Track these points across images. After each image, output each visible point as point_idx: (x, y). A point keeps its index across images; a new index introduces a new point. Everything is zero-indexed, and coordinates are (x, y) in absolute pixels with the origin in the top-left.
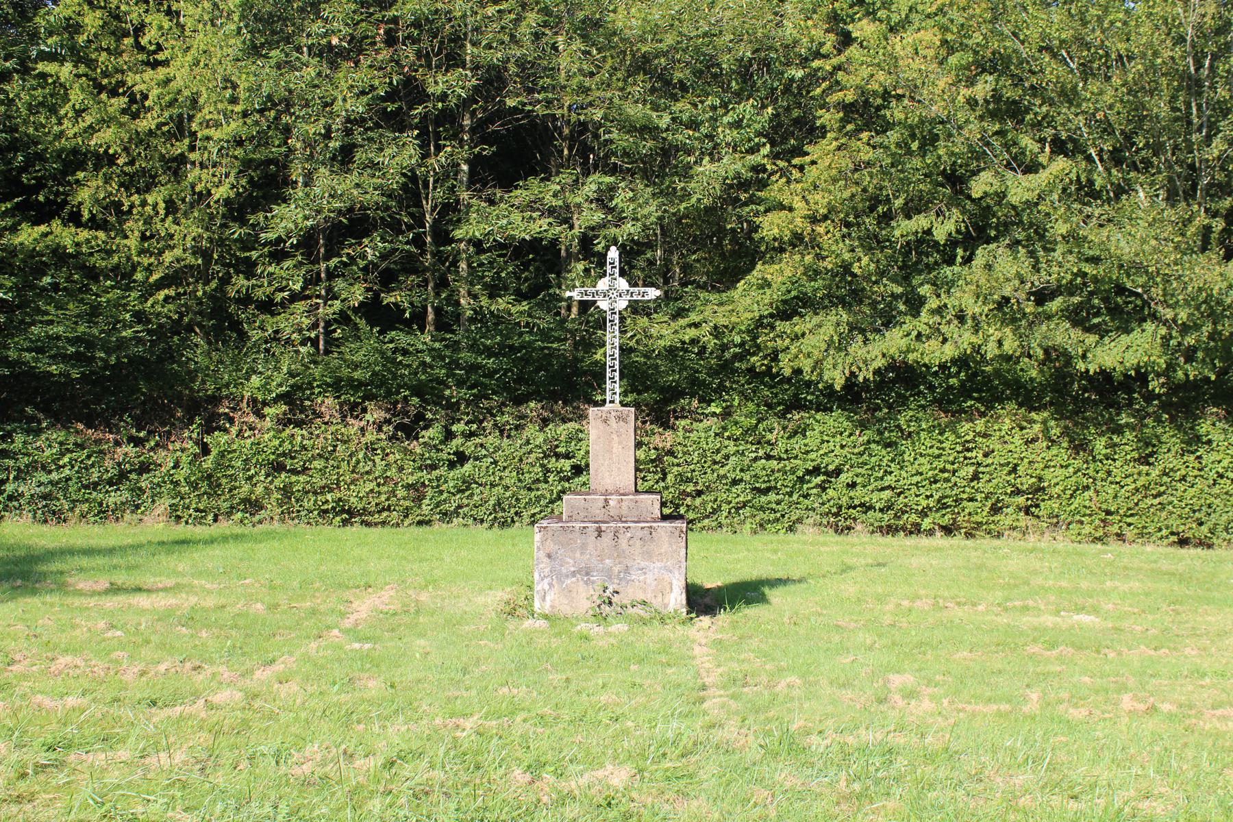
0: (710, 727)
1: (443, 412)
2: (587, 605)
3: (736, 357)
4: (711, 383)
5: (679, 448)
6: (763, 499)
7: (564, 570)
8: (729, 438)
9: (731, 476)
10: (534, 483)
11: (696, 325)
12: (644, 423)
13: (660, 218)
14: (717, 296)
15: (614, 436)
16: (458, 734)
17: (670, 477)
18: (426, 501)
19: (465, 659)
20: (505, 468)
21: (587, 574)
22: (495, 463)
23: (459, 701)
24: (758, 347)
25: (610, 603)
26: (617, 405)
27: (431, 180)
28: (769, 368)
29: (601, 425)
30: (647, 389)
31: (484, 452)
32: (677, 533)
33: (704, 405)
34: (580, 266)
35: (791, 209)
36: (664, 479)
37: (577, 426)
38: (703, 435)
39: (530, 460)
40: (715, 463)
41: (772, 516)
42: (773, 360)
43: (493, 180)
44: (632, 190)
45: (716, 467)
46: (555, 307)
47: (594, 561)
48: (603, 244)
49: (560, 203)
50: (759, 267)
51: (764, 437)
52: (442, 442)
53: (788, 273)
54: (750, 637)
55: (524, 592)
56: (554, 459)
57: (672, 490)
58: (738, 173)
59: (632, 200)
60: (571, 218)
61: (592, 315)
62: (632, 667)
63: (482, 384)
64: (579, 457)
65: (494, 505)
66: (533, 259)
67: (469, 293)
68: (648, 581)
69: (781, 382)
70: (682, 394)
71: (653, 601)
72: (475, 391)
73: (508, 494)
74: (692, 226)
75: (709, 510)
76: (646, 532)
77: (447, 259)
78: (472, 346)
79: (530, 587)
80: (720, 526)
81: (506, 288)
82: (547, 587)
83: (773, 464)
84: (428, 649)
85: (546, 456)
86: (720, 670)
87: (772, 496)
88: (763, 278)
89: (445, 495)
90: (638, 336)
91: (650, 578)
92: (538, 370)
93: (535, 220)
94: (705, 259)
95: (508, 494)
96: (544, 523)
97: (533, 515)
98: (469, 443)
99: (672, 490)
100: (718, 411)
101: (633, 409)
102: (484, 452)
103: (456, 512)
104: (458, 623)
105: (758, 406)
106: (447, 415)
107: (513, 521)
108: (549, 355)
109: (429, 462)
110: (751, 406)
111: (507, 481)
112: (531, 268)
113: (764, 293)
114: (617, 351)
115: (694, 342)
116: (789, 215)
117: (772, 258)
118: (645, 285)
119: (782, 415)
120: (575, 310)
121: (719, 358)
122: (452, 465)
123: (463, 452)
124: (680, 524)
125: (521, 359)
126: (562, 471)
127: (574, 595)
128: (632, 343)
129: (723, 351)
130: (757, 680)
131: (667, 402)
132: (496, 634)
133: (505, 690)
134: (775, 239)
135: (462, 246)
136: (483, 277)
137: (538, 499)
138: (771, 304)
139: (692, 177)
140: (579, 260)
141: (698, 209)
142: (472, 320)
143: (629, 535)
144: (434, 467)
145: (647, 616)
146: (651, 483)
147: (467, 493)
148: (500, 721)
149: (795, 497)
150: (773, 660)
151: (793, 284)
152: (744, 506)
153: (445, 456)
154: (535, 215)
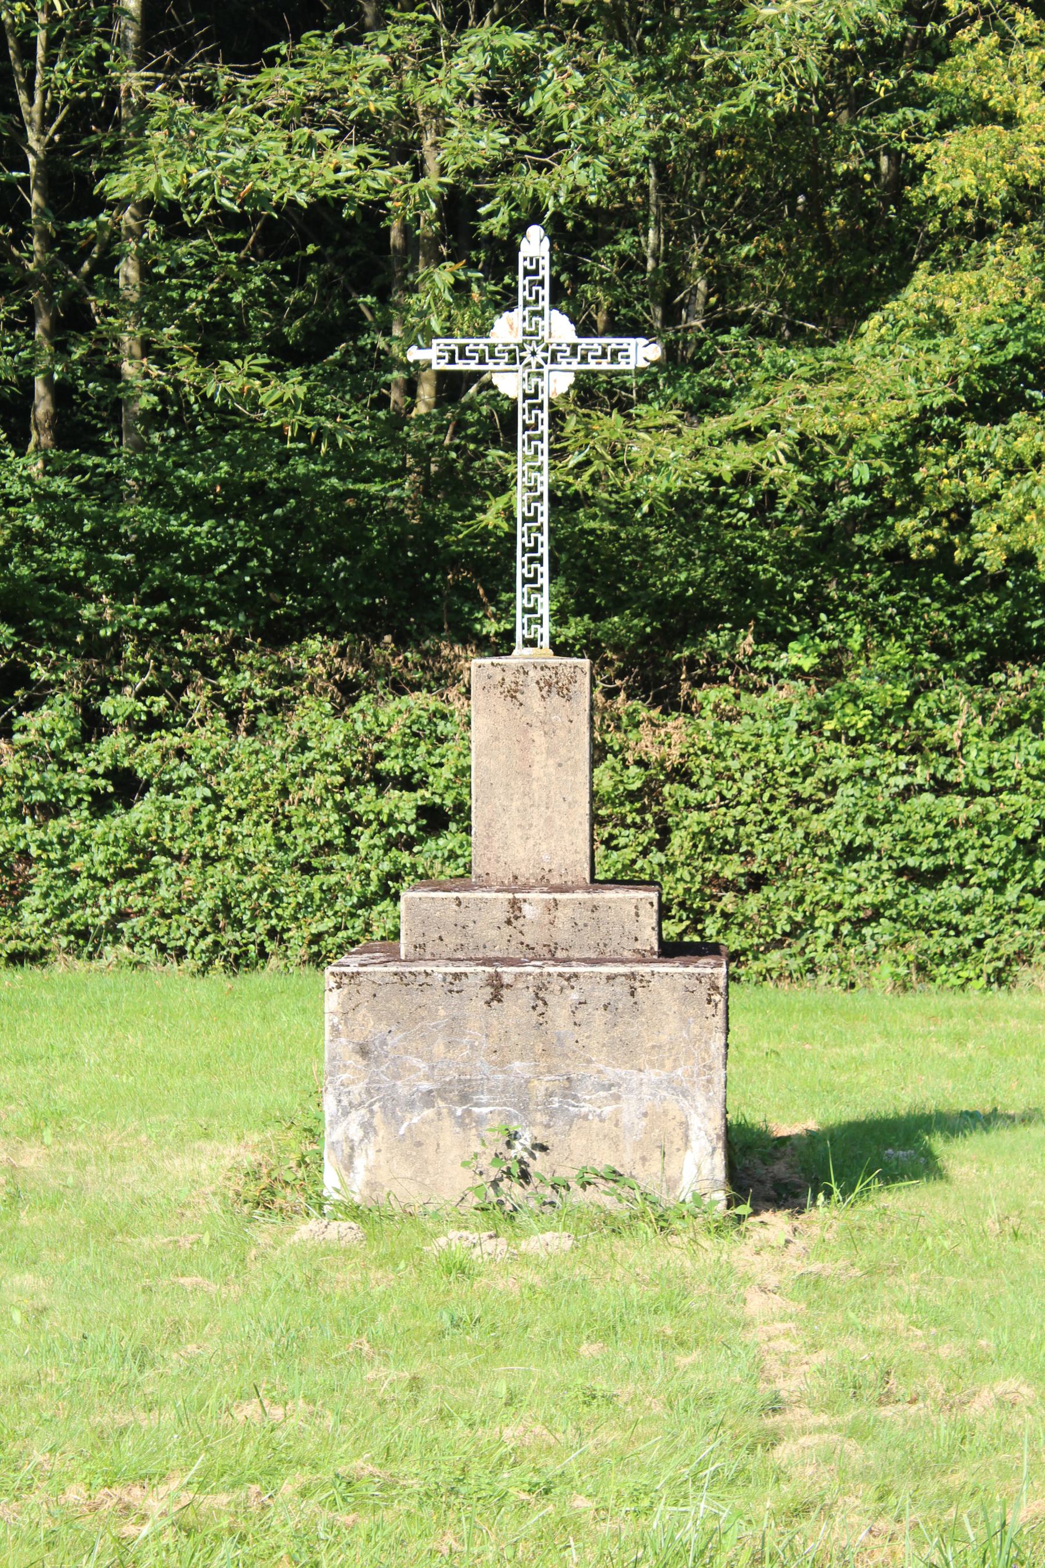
0: (796, 1513)
1: (78, 665)
2: (462, 1179)
3: (858, 520)
4: (788, 589)
5: (704, 761)
6: (927, 898)
7: (402, 1089)
8: (836, 736)
9: (842, 836)
10: (317, 852)
11: (751, 435)
12: (611, 694)
13: (657, 145)
14: (806, 356)
15: (537, 735)
16: (129, 1530)
17: (679, 840)
18: (32, 901)
19: (142, 1326)
20: (241, 813)
21: (464, 1098)
22: (216, 798)
23: (128, 1442)
24: (917, 494)
25: (525, 1176)
26: (544, 652)
27: (41, 36)
28: (946, 549)
29: (502, 706)
30: (618, 605)
31: (186, 770)
32: (702, 992)
33: (771, 648)
34: (444, 276)
35: (1010, 120)
36: (662, 844)
37: (433, 703)
38: (767, 727)
39: (307, 794)
40: (798, 801)
41: (951, 944)
42: (954, 528)
43: (207, 38)
44: (583, 69)
45: (802, 811)
46: (375, 385)
47: (482, 1063)
48: (503, 218)
49: (388, 104)
50: (920, 277)
51: (930, 733)
52: (73, 744)
53: (1000, 292)
54: (896, 1271)
55: (296, 1145)
56: (372, 790)
57: (683, 872)
58: (868, 21)
59: (581, 96)
60: (417, 144)
61: (471, 406)
62: (586, 1349)
63: (182, 591)
64: (439, 784)
65: (213, 913)
66: (316, 256)
67: (147, 347)
68: (625, 1119)
69: (976, 587)
70: (712, 619)
71: (639, 1171)
72: (162, 608)
73: (250, 882)
74: (741, 166)
75: (783, 926)
76: (621, 988)
77: (85, 253)
78: (153, 487)
79: (313, 1134)
80: (812, 968)
81: (243, 334)
82: (356, 1133)
83: (955, 804)
84: (45, 1299)
85: (350, 782)
86: (818, 1359)
87: (951, 892)
88: (931, 307)
89: (83, 884)
90: (597, 466)
91: (629, 1110)
92: (328, 553)
93: (321, 149)
94: (777, 255)
95: (250, 882)
96: (351, 963)
97: (317, 938)
98: (146, 748)
99: (683, 872)
100: (807, 663)
101: (586, 663)
102: (186, 770)
103: (112, 930)
104: (124, 1229)
105: (914, 648)
106: (88, 671)
107: (263, 954)
108: (359, 510)
109: (39, 796)
110: (896, 651)
111: (247, 848)
112: (310, 278)
113: (935, 349)
114: (544, 507)
115: (743, 479)
116: (1007, 137)
117: (956, 252)
118: (615, 329)
119: (980, 676)
120: (426, 392)
121: (811, 522)
122: (101, 805)
123: (130, 772)
124: (707, 967)
125: (284, 522)
126: (392, 821)
127: (429, 1152)
128: (581, 484)
129: (822, 504)
130: (917, 1386)
131: (671, 638)
132: (224, 1258)
133: (251, 1409)
134: (965, 203)
135: (127, 218)
136: (183, 303)
137: (330, 895)
138: (953, 377)
139: (744, 34)
140: (440, 259)
141: (756, 122)
142: (153, 419)
143: (574, 996)
144: (52, 810)
145: (621, 1211)
146: (629, 854)
147: (142, 879)
148: (240, 1494)
149: (1012, 892)
150: (958, 1332)
151: (1012, 323)
152: (876, 915)
153: (83, 782)
154: (322, 136)
